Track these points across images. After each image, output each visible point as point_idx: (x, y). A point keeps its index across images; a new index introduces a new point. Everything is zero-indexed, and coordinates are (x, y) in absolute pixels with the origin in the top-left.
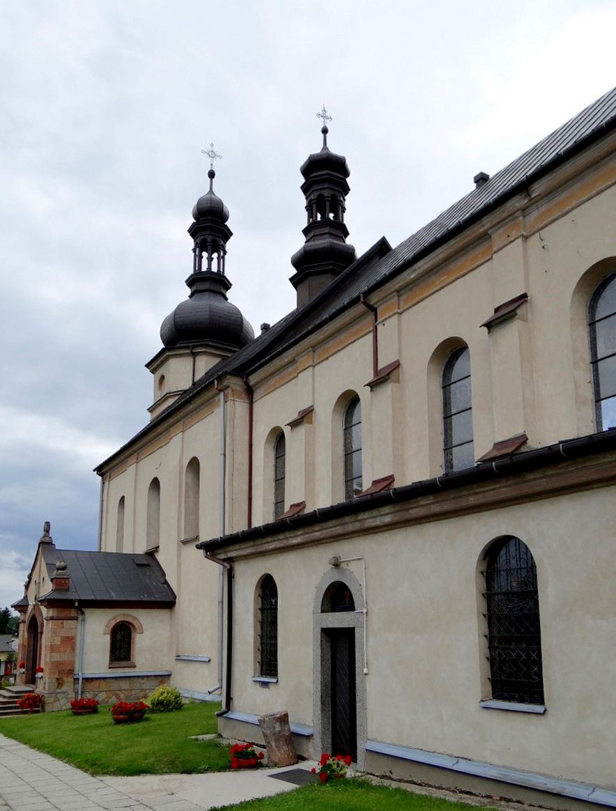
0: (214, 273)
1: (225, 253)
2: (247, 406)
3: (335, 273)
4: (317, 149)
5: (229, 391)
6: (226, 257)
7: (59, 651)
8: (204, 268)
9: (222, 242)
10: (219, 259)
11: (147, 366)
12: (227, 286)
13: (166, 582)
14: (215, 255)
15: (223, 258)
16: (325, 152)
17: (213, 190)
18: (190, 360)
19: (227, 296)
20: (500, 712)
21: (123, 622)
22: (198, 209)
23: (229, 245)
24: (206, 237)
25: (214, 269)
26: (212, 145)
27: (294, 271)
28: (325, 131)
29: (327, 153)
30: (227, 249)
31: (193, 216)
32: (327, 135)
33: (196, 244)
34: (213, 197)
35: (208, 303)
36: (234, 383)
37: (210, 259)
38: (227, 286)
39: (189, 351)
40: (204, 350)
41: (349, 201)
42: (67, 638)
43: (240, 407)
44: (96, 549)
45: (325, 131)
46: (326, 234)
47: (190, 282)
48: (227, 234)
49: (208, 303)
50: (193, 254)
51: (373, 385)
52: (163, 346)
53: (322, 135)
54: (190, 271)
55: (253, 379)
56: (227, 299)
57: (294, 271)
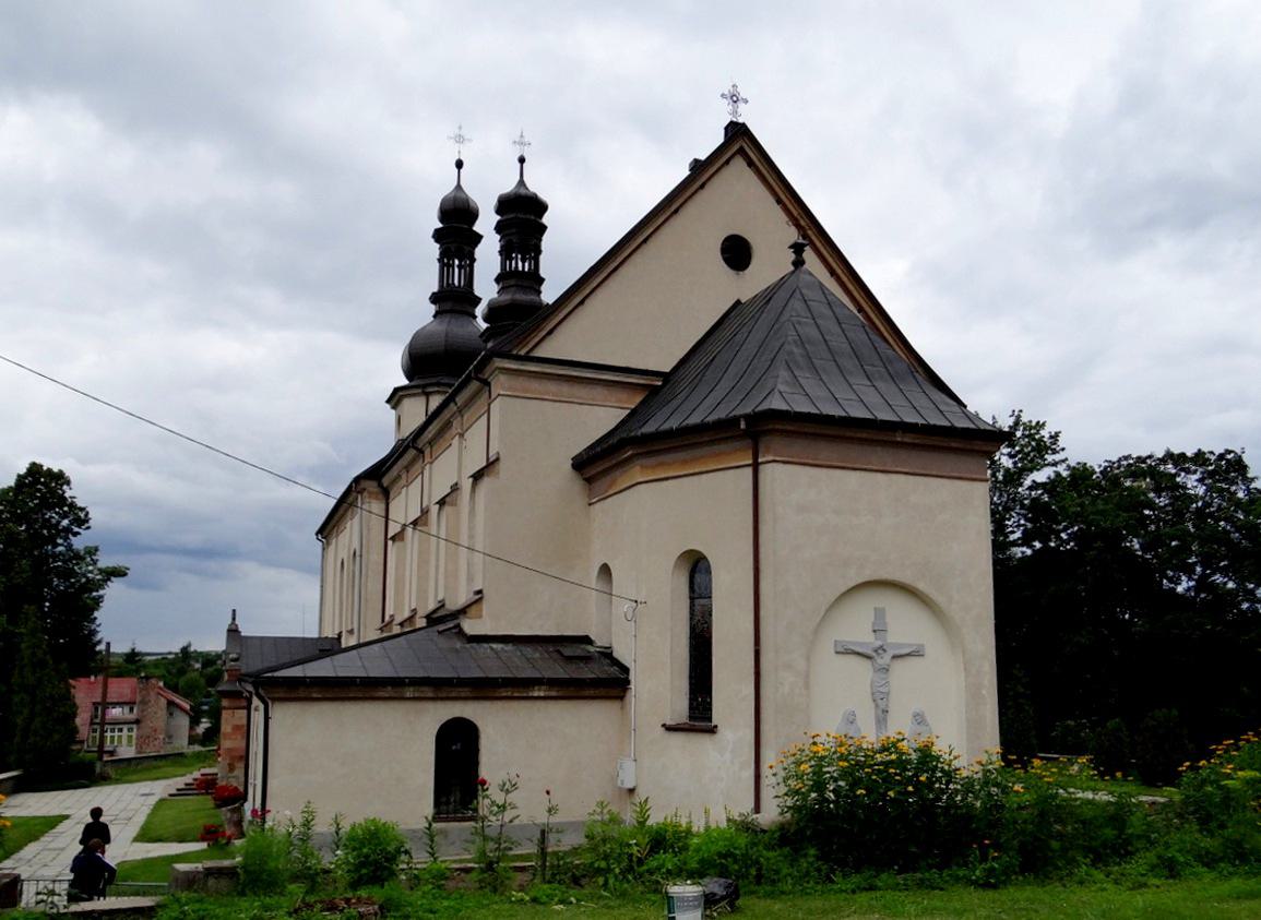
2: (383, 506)
3: (450, 386)
4: (508, 186)
5: (365, 494)
7: (230, 739)
11: (388, 402)
13: (876, 618)
17: (525, 179)
18: (423, 399)
24: (511, 237)
28: (522, 160)
31: (443, 200)
32: (525, 165)
36: (371, 485)
39: (420, 391)
40: (436, 389)
42: (237, 726)
43: (377, 507)
44: (316, 636)
45: (522, 160)
46: (512, 286)
50: (437, 265)
53: (519, 165)
55: (386, 481)
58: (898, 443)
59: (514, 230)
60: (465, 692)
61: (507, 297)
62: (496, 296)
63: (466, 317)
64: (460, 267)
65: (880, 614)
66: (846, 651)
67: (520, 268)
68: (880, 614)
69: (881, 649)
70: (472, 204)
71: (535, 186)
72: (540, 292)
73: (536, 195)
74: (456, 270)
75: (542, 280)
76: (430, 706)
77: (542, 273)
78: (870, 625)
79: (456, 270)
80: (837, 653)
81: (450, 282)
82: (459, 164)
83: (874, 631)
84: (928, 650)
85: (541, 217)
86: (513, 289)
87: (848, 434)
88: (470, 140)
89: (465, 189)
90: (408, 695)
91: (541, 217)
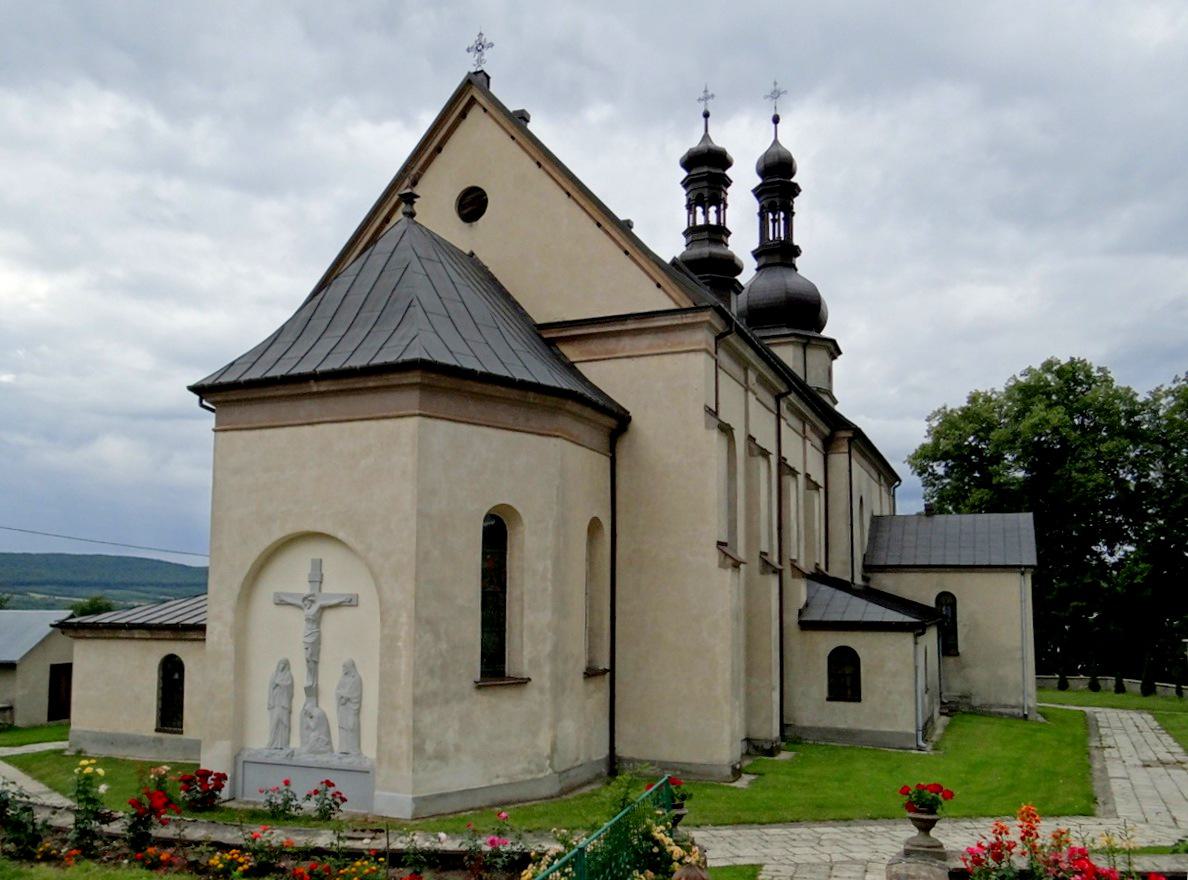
0: (712, 226)
2: (605, 462)
4: (694, 142)
16: (774, 150)
19: (797, 265)
20: (829, 470)
23: (798, 203)
25: (713, 221)
26: (491, 45)
28: (706, 115)
29: (778, 153)
32: (709, 119)
34: (710, 144)
35: (705, 250)
37: (706, 213)
48: (795, 190)
52: (668, 260)
53: (703, 120)
56: (796, 270)
60: (168, 634)
62: (684, 249)
63: (787, 269)
64: (774, 221)
65: (318, 565)
66: (281, 603)
68: (318, 565)
69: (309, 600)
71: (719, 141)
73: (726, 153)
74: (771, 225)
76: (154, 644)
78: (307, 577)
79: (771, 225)
80: (277, 604)
81: (777, 236)
83: (310, 582)
84: (362, 600)
89: (712, 139)
90: (137, 636)
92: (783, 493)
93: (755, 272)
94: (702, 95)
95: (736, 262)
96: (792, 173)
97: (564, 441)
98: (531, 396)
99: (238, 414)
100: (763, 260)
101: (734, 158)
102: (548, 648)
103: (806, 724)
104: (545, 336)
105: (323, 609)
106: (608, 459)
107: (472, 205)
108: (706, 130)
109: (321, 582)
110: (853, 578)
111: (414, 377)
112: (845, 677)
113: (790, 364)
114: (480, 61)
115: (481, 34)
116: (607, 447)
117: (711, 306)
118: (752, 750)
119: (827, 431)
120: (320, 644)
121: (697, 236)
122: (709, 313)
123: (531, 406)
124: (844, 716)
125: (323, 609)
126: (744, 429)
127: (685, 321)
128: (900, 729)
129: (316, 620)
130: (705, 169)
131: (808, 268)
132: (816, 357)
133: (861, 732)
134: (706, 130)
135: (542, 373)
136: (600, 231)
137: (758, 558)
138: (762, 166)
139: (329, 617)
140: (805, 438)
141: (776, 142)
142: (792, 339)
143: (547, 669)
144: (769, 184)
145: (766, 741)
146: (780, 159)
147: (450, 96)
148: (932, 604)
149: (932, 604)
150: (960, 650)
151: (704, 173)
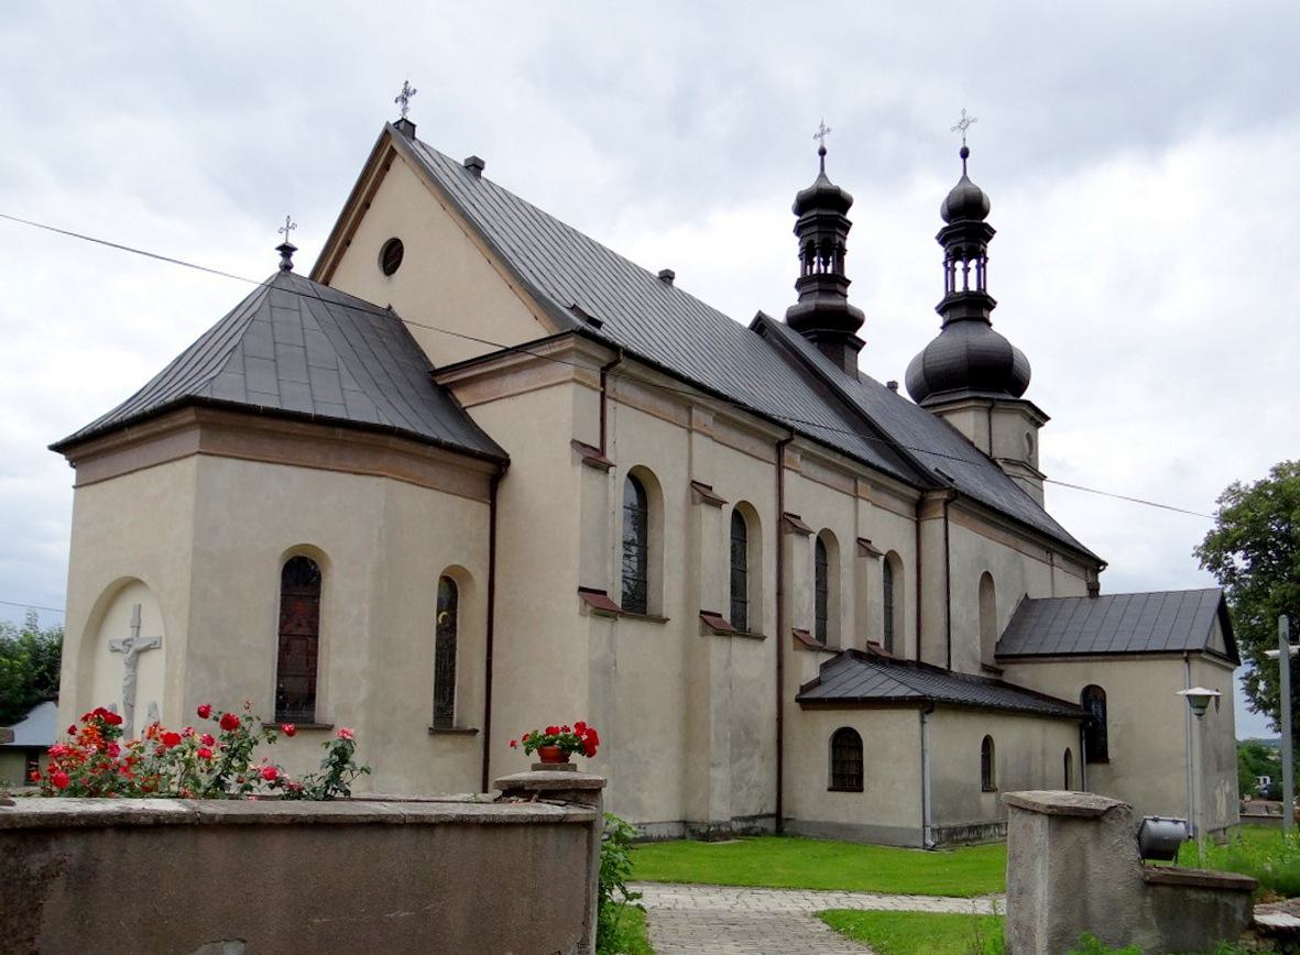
1: (986, 259)
2: (486, 509)
4: (807, 182)
6: (988, 265)
8: (959, 288)
9: (982, 247)
10: (978, 267)
12: (989, 304)
14: (973, 264)
15: (984, 266)
17: (968, 174)
19: (991, 321)
21: (459, 566)
22: (949, 210)
23: (992, 248)
24: (959, 245)
27: (860, 334)
28: (823, 152)
30: (988, 255)
32: (826, 157)
33: (948, 255)
35: (970, 337)
38: (989, 304)
41: (852, 242)
45: (823, 152)
47: (942, 310)
48: (987, 233)
49: (970, 337)
50: (943, 269)
51: (717, 503)
53: (819, 158)
54: (940, 296)
56: (990, 325)
57: (860, 334)
58: (427, 458)
59: (963, 238)
61: (811, 303)
67: (823, 271)
70: (985, 202)
71: (838, 180)
72: (846, 296)
75: (848, 282)
77: (848, 274)
82: (965, 154)
85: (845, 213)
86: (817, 293)
87: (939, 475)
88: (953, 129)
91: (845, 212)
92: (785, 554)
93: (941, 331)
94: (818, 131)
95: (851, 313)
96: (985, 213)
97: (390, 480)
98: (340, 432)
99: (101, 467)
100: (948, 317)
101: (854, 197)
102: (363, 695)
103: (807, 818)
104: (440, 383)
105: (139, 652)
106: (488, 507)
107: (392, 256)
108: (822, 169)
109: (139, 627)
110: (949, 666)
111: (189, 416)
112: (847, 767)
113: (970, 434)
114: (405, 110)
115: (407, 82)
116: (487, 491)
117: (572, 331)
118: (688, 834)
119: (914, 494)
120: (135, 688)
121: (807, 288)
122: (572, 339)
123: (343, 443)
124: (845, 809)
125: (139, 652)
126: (686, 474)
127: (554, 350)
128: (904, 825)
129: (133, 664)
130: (814, 212)
131: (1005, 323)
132: (1008, 427)
133: (862, 827)
134: (822, 169)
135: (434, 425)
136: (490, 267)
137: (698, 618)
138: (946, 211)
139: (144, 658)
140: (856, 497)
141: (965, 178)
142: (972, 403)
143: (360, 718)
144: (956, 226)
145: (703, 823)
146: (966, 197)
147: (374, 143)
148: (1077, 700)
149: (1077, 700)
150: (1110, 757)
151: (812, 217)
